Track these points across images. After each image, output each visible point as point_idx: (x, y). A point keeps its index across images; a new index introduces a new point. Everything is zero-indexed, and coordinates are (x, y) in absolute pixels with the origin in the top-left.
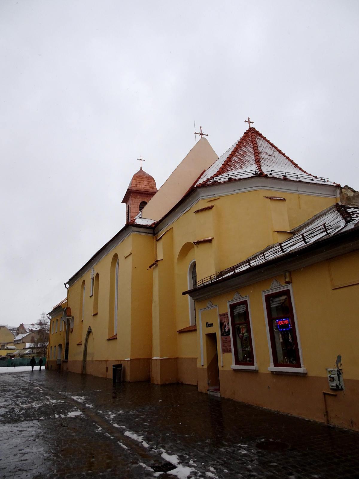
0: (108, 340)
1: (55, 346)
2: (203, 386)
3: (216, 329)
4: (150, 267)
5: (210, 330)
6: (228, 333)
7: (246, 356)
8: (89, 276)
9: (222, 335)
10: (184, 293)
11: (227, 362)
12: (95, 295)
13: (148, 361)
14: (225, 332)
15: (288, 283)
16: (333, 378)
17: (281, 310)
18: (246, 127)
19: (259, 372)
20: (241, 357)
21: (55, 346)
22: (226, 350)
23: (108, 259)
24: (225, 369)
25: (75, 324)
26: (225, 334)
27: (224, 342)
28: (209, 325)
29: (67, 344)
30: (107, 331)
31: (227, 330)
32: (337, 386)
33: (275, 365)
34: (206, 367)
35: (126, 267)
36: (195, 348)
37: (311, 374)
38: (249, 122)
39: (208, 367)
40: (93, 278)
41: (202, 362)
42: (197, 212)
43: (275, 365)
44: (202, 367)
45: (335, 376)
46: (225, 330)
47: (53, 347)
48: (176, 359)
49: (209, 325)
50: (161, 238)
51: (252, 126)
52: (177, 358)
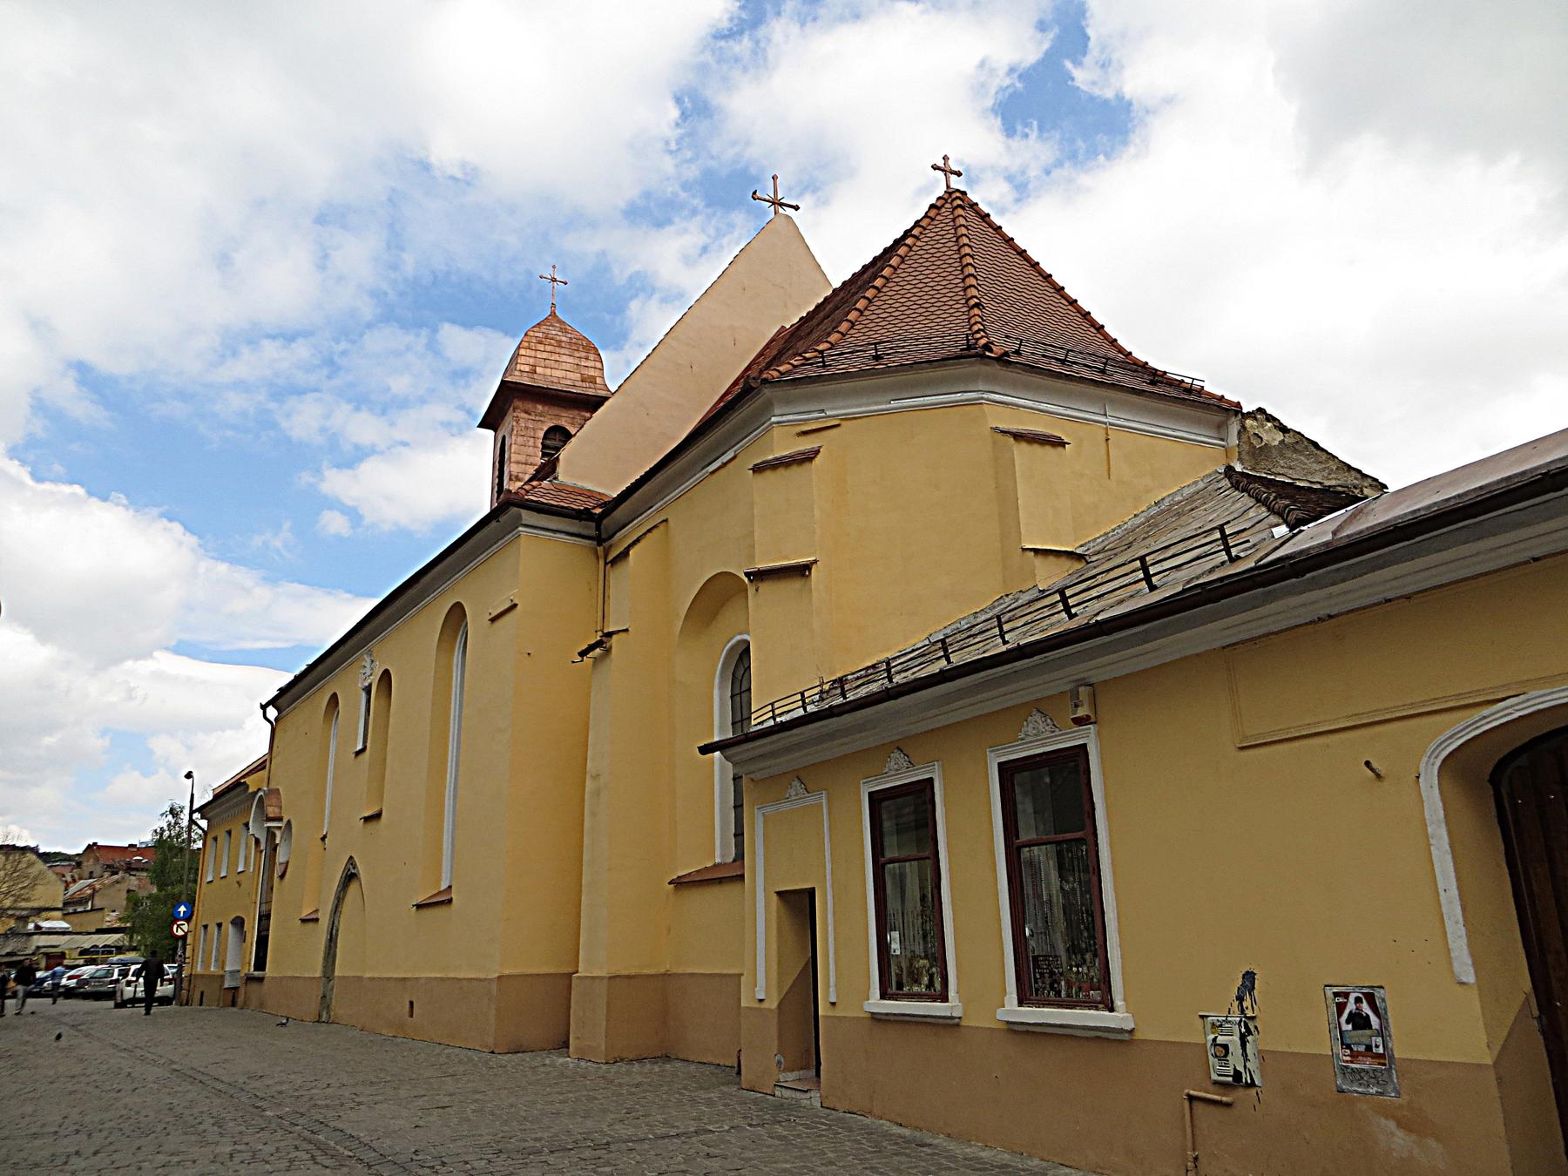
17: (1053, 801)
24: (839, 1012)
29: (265, 918)
38: (947, 171)
41: (762, 986)
42: (757, 469)
51: (956, 183)
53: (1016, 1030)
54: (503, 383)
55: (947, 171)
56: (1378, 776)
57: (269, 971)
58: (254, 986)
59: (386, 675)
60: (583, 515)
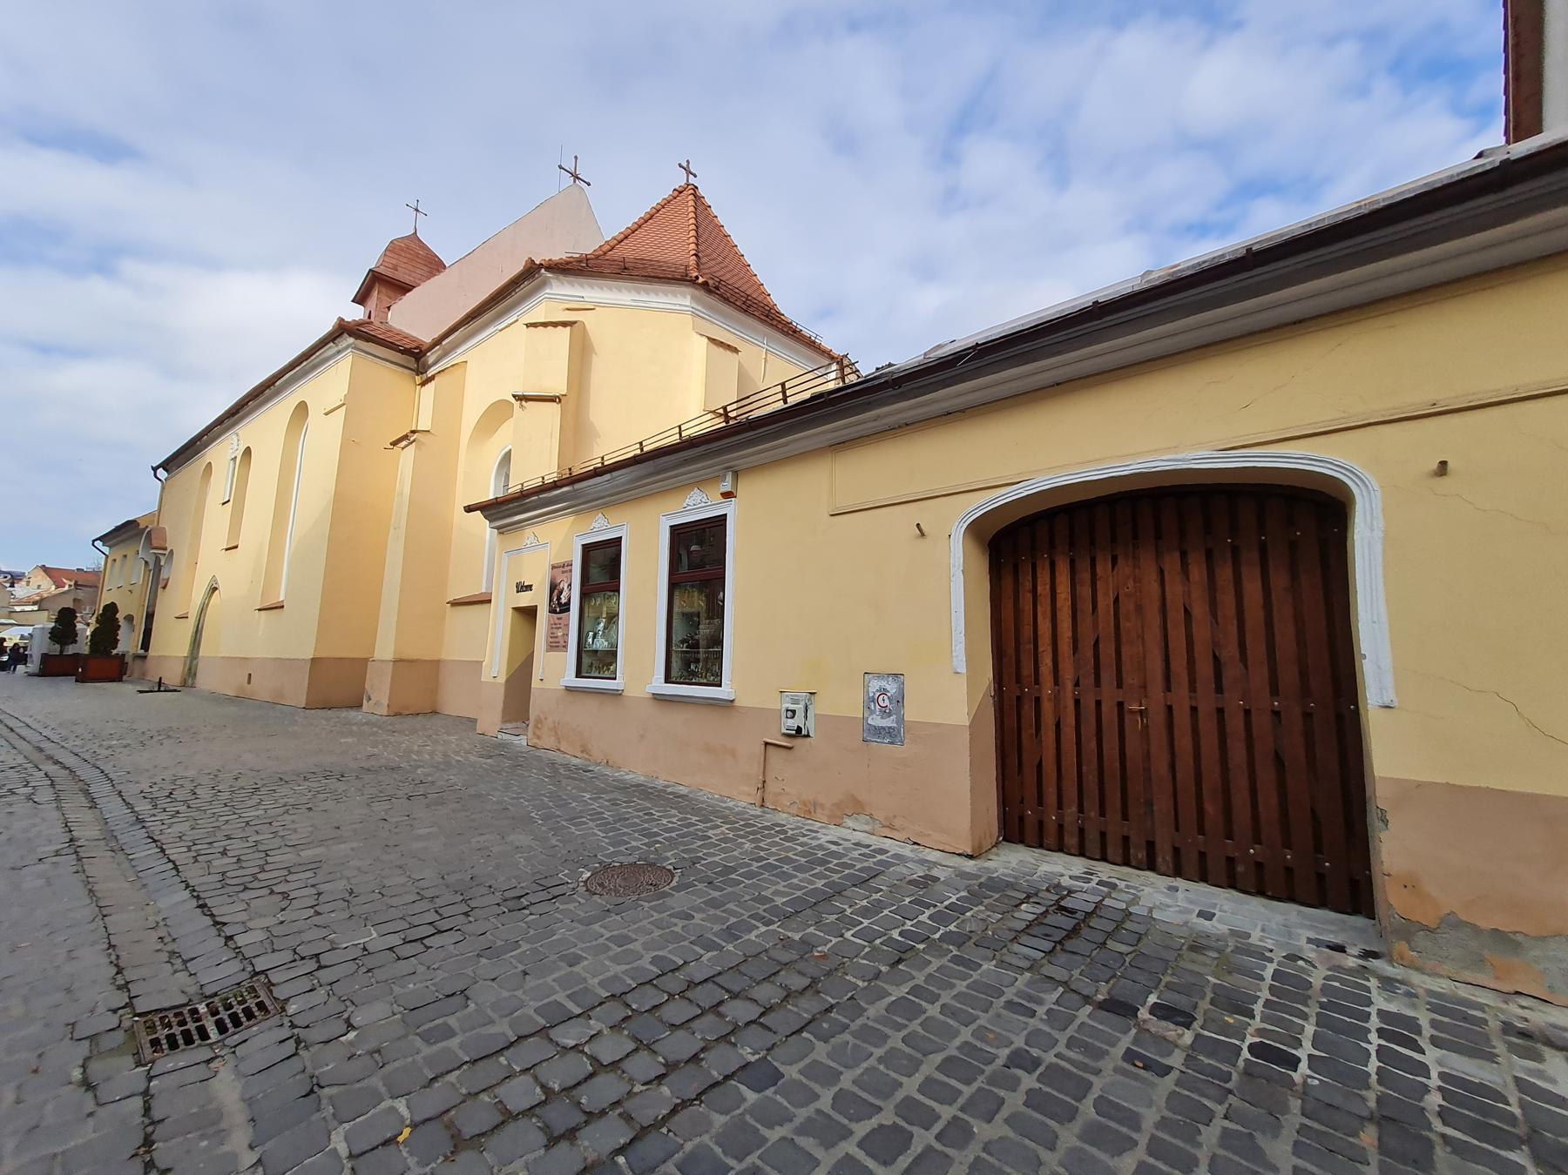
2: (490, 721)
3: (539, 598)
4: (394, 444)
5: (525, 600)
6: (565, 608)
7: (596, 661)
8: (221, 453)
9: (552, 611)
10: (469, 509)
11: (556, 670)
12: (236, 502)
13: (359, 666)
14: (560, 604)
15: (728, 495)
16: (794, 712)
17: (698, 556)
18: (680, 180)
20: (675, 673)
22: (556, 645)
23: (278, 412)
24: (546, 685)
25: (175, 572)
26: (559, 608)
27: (553, 627)
28: (523, 588)
29: (150, 617)
31: (563, 601)
32: (799, 730)
34: (502, 679)
35: (325, 434)
36: (487, 645)
38: (689, 172)
39: (508, 681)
41: (496, 668)
42: (528, 325)
45: (799, 708)
46: (559, 599)
48: (436, 664)
49: (523, 588)
50: (432, 378)
51: (692, 180)
53: (659, 698)
54: (618, 591)
55: (689, 172)
56: (923, 534)
57: (152, 652)
58: (138, 662)
59: (248, 451)
60: (406, 352)
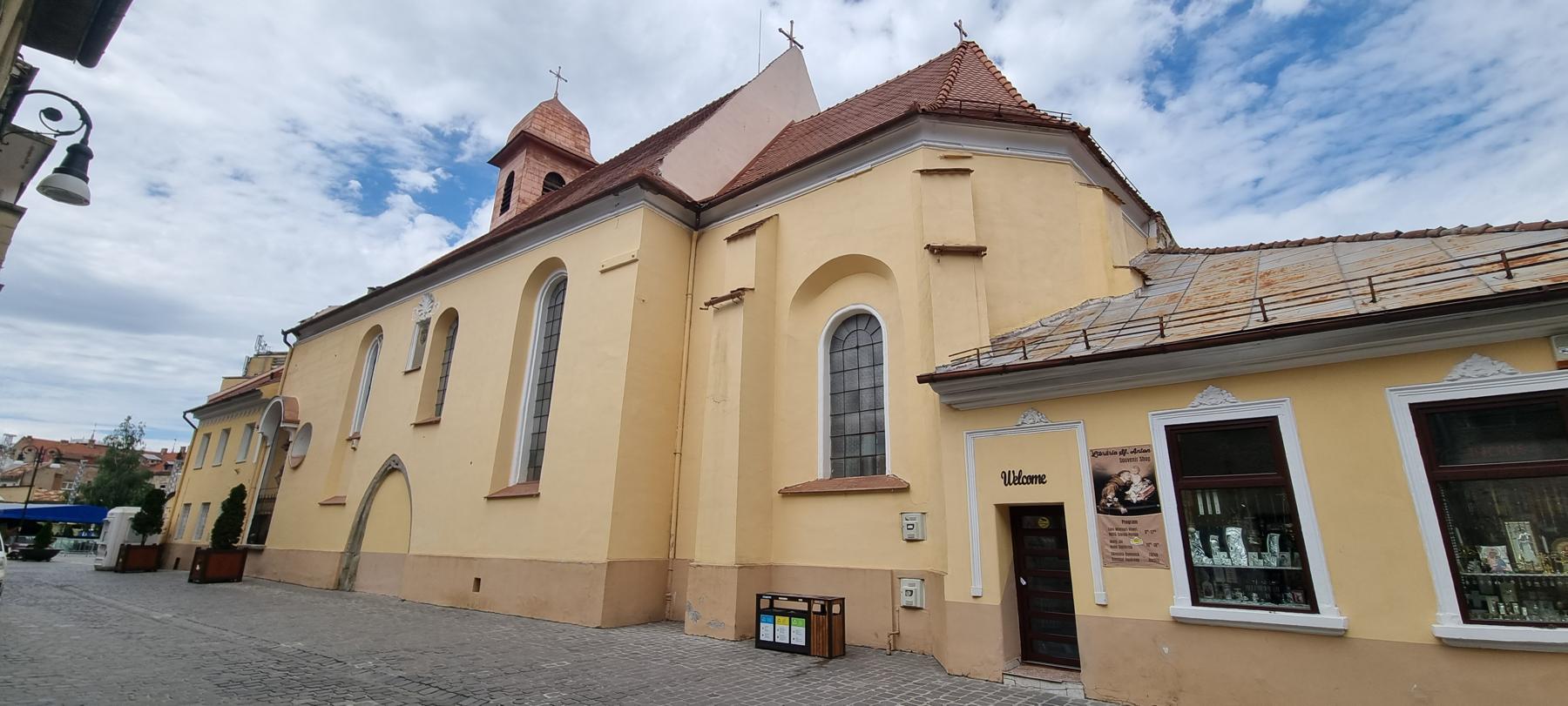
0: (489, 498)
1: (206, 505)
19: (1350, 635)
21: (206, 505)
23: (359, 329)
30: (488, 470)
33: (1195, 602)
37: (1363, 631)
40: (425, 324)
42: (730, 240)
43: (1195, 602)
44: (1100, 613)
47: (196, 509)
52: (770, 567)
